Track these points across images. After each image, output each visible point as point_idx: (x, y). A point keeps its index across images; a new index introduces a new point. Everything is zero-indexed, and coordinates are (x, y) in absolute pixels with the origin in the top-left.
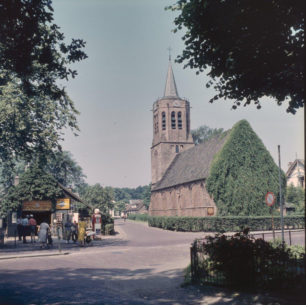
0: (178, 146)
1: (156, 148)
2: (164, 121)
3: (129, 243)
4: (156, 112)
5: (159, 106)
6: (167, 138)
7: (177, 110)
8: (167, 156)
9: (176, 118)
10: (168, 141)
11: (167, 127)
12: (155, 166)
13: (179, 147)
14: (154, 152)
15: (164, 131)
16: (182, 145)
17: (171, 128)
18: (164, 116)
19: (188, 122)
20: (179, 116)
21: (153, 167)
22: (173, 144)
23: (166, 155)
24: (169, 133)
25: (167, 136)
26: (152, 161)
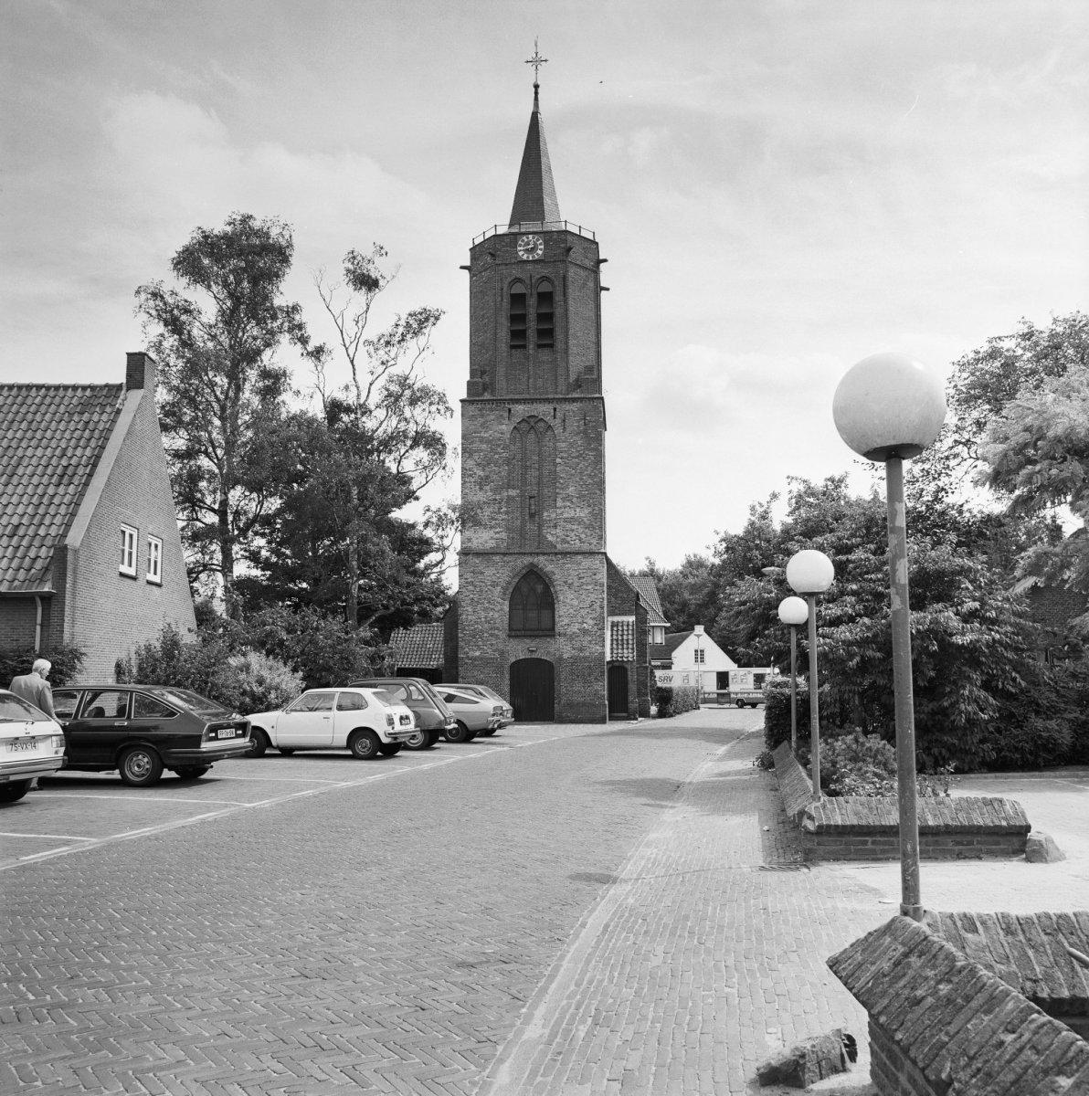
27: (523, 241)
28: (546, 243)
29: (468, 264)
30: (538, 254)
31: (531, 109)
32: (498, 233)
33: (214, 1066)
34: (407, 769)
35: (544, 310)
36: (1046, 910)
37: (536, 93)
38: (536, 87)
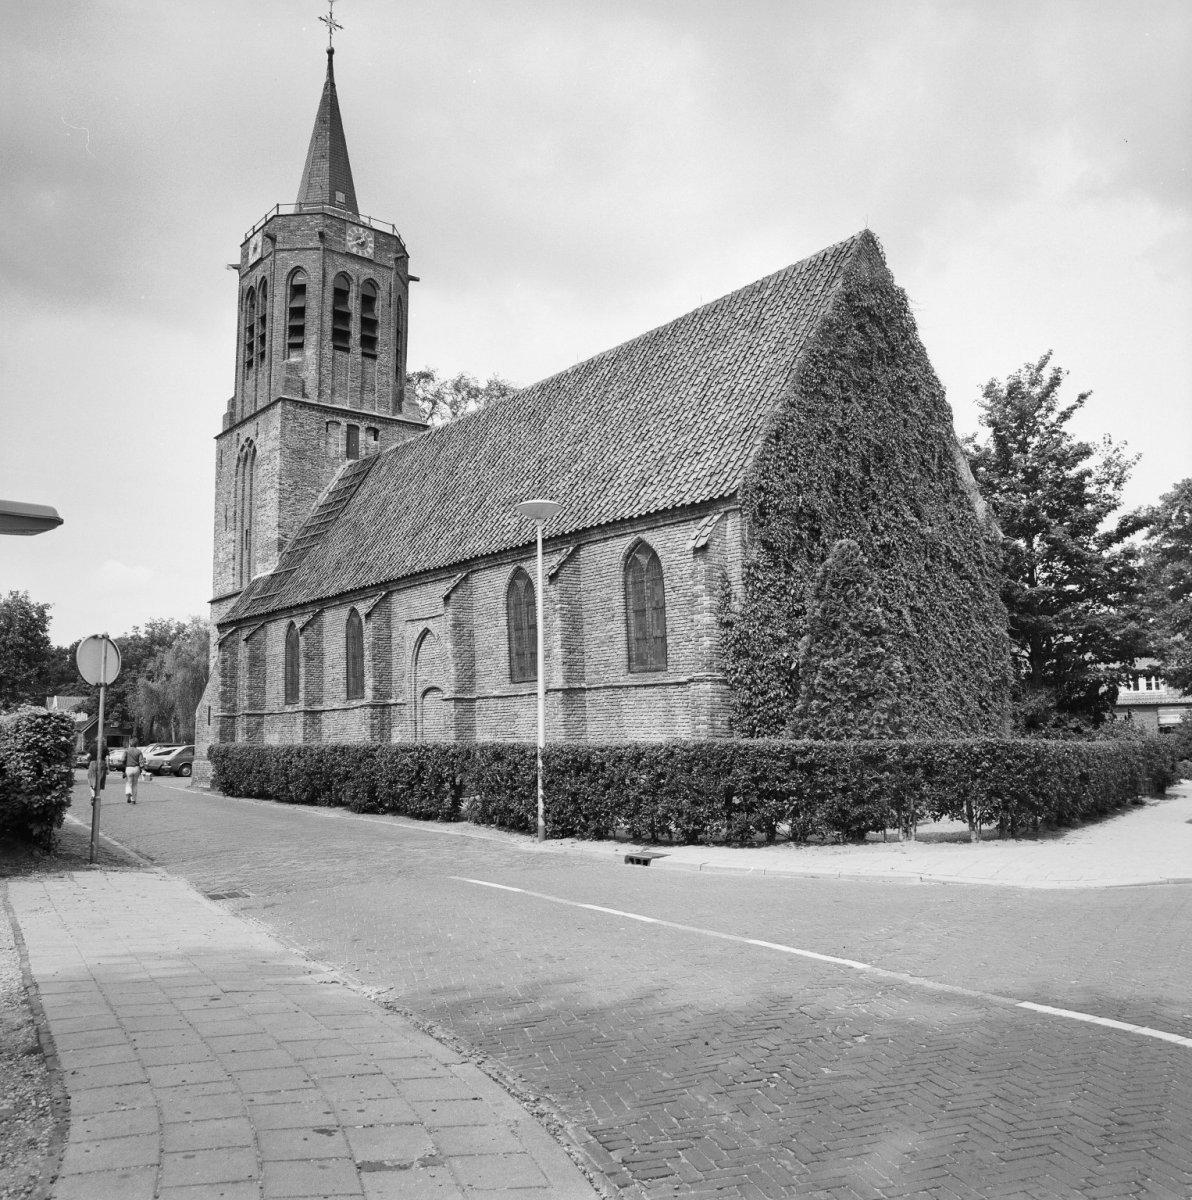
0: (358, 428)
1: (247, 431)
2: (298, 313)
3: (244, 467)
4: (259, 273)
5: (279, 238)
6: (311, 387)
7: (360, 273)
8: (309, 466)
9: (354, 305)
10: (313, 400)
11: (311, 339)
12: (236, 517)
13: (362, 436)
14: (235, 452)
15: (294, 358)
16: (373, 425)
17: (328, 344)
18: (299, 290)
19: (401, 335)
20: (368, 302)
21: (224, 520)
22: (339, 419)
23: (301, 459)
24: (320, 366)
25: (310, 375)
26: (218, 495)
27: (353, 231)
28: (376, 241)
29: (411, 284)
30: (368, 253)
31: (323, 78)
32: (280, 213)
33: (872, 469)
34: (371, 820)
35: (296, 304)
36: (952, 406)
37: (330, 60)
38: (331, 52)
